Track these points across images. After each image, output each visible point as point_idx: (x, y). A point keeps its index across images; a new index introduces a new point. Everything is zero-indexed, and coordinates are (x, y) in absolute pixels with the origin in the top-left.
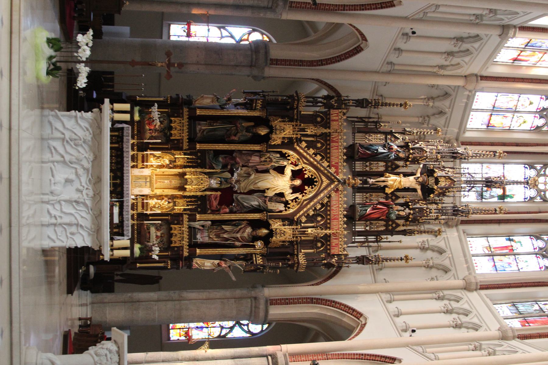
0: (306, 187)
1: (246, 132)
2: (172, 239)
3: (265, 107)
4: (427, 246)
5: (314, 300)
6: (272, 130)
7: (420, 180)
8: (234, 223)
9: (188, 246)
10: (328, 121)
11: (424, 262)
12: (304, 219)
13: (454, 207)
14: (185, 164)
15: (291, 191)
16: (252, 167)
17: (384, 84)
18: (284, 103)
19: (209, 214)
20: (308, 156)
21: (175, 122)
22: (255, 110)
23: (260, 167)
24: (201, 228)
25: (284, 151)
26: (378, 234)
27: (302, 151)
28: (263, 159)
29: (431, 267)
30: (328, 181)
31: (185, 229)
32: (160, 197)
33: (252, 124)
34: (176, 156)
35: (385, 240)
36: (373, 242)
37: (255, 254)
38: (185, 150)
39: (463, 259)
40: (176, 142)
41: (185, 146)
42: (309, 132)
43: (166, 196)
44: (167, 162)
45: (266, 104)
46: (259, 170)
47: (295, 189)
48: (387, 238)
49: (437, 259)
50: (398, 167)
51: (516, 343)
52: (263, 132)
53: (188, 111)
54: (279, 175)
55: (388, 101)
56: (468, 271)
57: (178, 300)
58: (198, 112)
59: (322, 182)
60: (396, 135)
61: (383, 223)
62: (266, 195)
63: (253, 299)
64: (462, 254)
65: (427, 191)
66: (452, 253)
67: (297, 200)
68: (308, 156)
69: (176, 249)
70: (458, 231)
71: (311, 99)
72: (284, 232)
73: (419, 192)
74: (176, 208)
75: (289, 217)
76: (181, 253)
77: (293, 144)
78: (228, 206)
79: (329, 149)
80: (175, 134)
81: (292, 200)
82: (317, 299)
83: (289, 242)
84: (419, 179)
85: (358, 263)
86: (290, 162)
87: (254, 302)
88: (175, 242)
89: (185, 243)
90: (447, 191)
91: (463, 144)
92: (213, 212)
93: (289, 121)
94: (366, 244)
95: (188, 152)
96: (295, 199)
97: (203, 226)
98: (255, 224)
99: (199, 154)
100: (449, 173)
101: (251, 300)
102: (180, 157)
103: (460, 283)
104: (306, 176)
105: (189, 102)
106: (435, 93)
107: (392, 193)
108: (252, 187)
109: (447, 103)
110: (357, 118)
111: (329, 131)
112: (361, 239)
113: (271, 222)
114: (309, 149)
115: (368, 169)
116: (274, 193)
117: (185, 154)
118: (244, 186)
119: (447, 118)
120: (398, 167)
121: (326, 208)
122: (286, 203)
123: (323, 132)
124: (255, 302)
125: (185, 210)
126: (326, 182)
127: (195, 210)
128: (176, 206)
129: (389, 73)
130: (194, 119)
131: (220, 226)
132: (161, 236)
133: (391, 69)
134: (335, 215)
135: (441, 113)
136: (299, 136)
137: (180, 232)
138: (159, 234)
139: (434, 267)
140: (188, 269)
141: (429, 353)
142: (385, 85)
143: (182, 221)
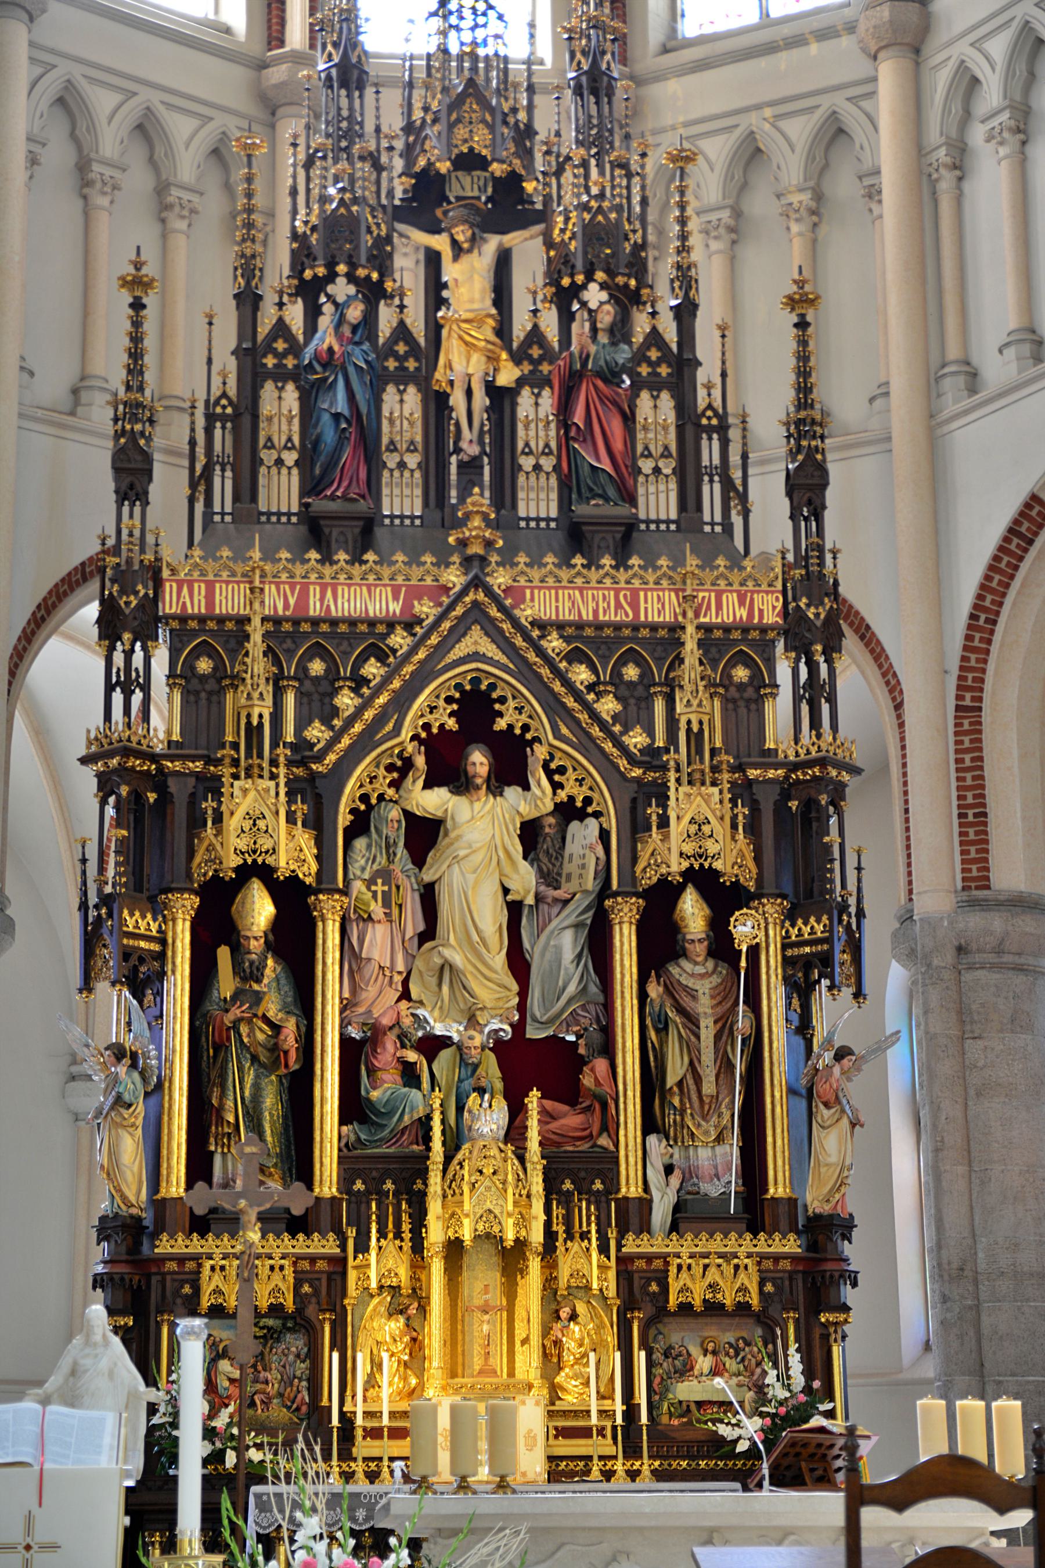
0: (501, 724)
1: (259, 981)
2: (728, 1302)
3: (152, 899)
4: (725, 215)
5: (967, 702)
6: (257, 870)
7: (462, 233)
8: (653, 1034)
9: (755, 1235)
10: (211, 625)
11: (795, 228)
12: (636, 739)
13: (578, 91)
14: (407, 1245)
15: (512, 793)
16: (410, 958)
17: (26, 375)
18: (133, 812)
19: (617, 1145)
20: (369, 715)
21: (218, 1291)
22: (163, 942)
23: (413, 921)
24: (675, 1181)
25: (344, 819)
26: (689, 423)
27: (346, 741)
28: (377, 909)
29: (819, 196)
30: (476, 632)
31: (684, 1246)
32: (552, 1358)
33: (224, 953)
34: (374, 1285)
35: (717, 393)
36: (725, 443)
37: (784, 947)
38: (343, 1247)
39: (783, 55)
40: (306, 1288)
41: (324, 1245)
42: (263, 709)
43: (546, 1331)
44: (396, 1325)
45: (148, 888)
46: (421, 927)
47: (510, 769)
48: (709, 387)
49: (790, 166)
50: (402, 331)
52: (260, 910)
53: (172, 1236)
54: (442, 842)
55: (111, 367)
56: (837, 35)
57: (976, 1282)
59: (475, 656)
60: (263, 330)
61: (645, 399)
62: (530, 900)
63: (965, 960)
64: (763, 63)
65: (508, 206)
66: (758, 107)
67: (553, 766)
68: (369, 715)
69: (769, 1288)
70: (660, 77)
71: (118, 697)
72: (692, 821)
73: (510, 239)
74: (595, 1286)
75: (627, 804)
76: (785, 1265)
77: (313, 776)
78: (581, 1062)
79: (334, 622)
81: (556, 786)
82: (959, 688)
83: (733, 801)
84: (460, 238)
85: (817, 513)
86: (391, 792)
87: (978, 958)
88: (743, 1289)
89: (744, 1246)
90: (511, 120)
91: (276, 36)
92: (610, 1126)
93: (218, 795)
94: (737, 475)
95: (351, 1233)
96: (549, 773)
97: (669, 1170)
98: (660, 945)
99: (359, 1186)
100: (435, 106)
101: (971, 968)
103: (889, 75)
104: (451, 724)
105: (125, 1232)
106: (59, 155)
107: (517, 358)
108: (499, 960)
109: (102, 101)
110: (192, 501)
111: (256, 621)
112: (711, 494)
113: (649, 879)
114: (335, 712)
115: (412, 460)
116: (524, 866)
117: (362, 1247)
118: (493, 990)
119: (169, 106)
120: (402, 331)
121: (586, 640)
122: (569, 812)
123: (261, 647)
124: (979, 951)
125: (603, 1249)
126: (476, 641)
127: (600, 1201)
128: (588, 1288)
131: (665, 1093)
132: (714, 1353)
134: (618, 605)
135: (146, 130)
136: (283, 753)
137: (697, 1270)
138: (704, 1363)
139: (818, 184)
140: (855, 1233)
142: (32, 374)
143: (649, 1258)
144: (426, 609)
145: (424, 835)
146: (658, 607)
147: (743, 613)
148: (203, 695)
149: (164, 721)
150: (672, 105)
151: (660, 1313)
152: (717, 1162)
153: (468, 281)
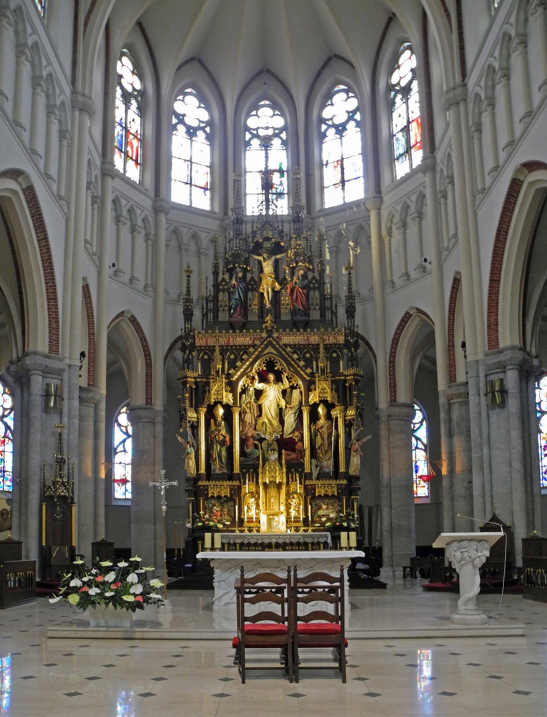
26: (323, 297)
30: (270, 347)
31: (320, 483)
47: (278, 380)
51: (439, 155)
52: (221, 411)
58: (203, 470)
80: (225, 492)
92: (303, 457)
98: (314, 417)
102: (247, 488)
106: (174, 243)
126: (270, 349)
129: (155, 289)
130: (209, 475)
133: (151, 287)
135: (195, 236)
141: (448, 243)
144: (257, 342)
145: (259, 394)
146: (314, 339)
147: (335, 341)
150: (322, 223)
151: (314, 498)
152: (328, 464)
153: (268, 267)
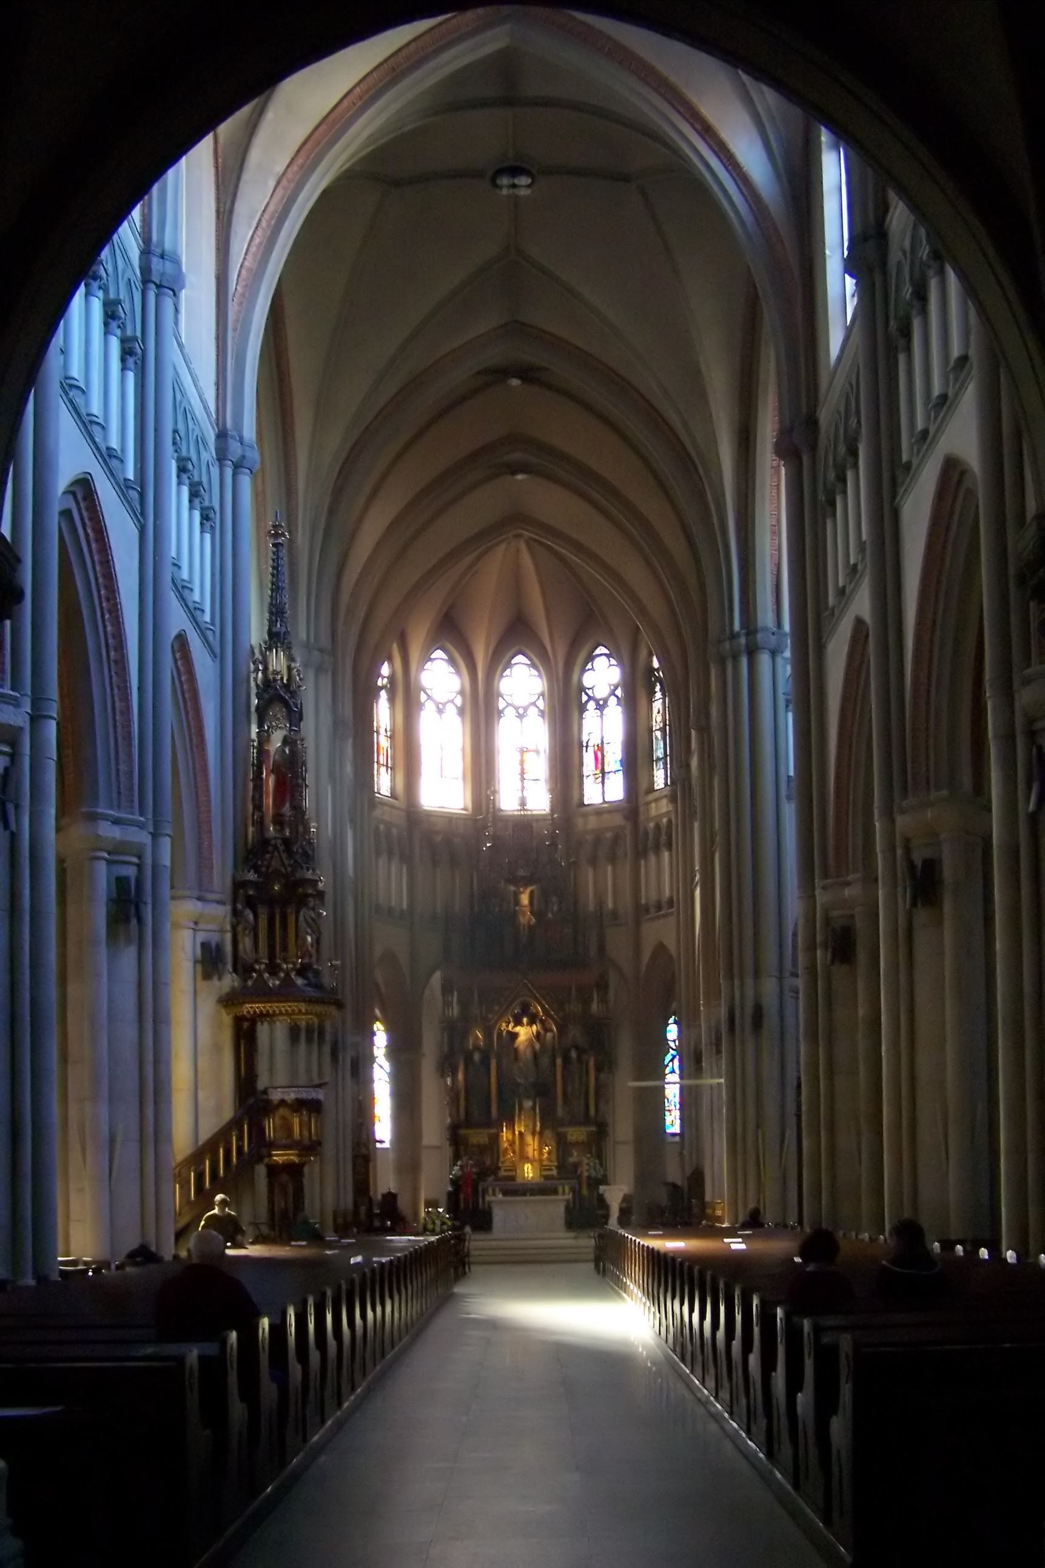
52: (477, 1057)
130: (469, 1123)
148: (464, 1005)
149: (455, 1011)
